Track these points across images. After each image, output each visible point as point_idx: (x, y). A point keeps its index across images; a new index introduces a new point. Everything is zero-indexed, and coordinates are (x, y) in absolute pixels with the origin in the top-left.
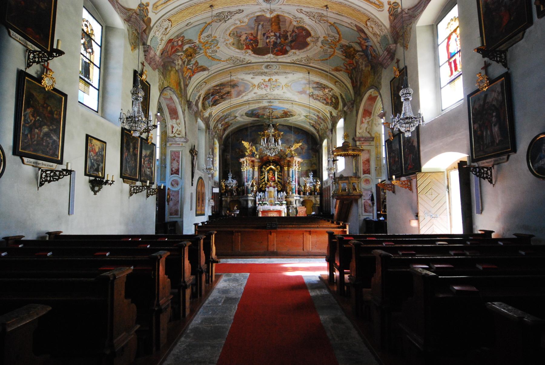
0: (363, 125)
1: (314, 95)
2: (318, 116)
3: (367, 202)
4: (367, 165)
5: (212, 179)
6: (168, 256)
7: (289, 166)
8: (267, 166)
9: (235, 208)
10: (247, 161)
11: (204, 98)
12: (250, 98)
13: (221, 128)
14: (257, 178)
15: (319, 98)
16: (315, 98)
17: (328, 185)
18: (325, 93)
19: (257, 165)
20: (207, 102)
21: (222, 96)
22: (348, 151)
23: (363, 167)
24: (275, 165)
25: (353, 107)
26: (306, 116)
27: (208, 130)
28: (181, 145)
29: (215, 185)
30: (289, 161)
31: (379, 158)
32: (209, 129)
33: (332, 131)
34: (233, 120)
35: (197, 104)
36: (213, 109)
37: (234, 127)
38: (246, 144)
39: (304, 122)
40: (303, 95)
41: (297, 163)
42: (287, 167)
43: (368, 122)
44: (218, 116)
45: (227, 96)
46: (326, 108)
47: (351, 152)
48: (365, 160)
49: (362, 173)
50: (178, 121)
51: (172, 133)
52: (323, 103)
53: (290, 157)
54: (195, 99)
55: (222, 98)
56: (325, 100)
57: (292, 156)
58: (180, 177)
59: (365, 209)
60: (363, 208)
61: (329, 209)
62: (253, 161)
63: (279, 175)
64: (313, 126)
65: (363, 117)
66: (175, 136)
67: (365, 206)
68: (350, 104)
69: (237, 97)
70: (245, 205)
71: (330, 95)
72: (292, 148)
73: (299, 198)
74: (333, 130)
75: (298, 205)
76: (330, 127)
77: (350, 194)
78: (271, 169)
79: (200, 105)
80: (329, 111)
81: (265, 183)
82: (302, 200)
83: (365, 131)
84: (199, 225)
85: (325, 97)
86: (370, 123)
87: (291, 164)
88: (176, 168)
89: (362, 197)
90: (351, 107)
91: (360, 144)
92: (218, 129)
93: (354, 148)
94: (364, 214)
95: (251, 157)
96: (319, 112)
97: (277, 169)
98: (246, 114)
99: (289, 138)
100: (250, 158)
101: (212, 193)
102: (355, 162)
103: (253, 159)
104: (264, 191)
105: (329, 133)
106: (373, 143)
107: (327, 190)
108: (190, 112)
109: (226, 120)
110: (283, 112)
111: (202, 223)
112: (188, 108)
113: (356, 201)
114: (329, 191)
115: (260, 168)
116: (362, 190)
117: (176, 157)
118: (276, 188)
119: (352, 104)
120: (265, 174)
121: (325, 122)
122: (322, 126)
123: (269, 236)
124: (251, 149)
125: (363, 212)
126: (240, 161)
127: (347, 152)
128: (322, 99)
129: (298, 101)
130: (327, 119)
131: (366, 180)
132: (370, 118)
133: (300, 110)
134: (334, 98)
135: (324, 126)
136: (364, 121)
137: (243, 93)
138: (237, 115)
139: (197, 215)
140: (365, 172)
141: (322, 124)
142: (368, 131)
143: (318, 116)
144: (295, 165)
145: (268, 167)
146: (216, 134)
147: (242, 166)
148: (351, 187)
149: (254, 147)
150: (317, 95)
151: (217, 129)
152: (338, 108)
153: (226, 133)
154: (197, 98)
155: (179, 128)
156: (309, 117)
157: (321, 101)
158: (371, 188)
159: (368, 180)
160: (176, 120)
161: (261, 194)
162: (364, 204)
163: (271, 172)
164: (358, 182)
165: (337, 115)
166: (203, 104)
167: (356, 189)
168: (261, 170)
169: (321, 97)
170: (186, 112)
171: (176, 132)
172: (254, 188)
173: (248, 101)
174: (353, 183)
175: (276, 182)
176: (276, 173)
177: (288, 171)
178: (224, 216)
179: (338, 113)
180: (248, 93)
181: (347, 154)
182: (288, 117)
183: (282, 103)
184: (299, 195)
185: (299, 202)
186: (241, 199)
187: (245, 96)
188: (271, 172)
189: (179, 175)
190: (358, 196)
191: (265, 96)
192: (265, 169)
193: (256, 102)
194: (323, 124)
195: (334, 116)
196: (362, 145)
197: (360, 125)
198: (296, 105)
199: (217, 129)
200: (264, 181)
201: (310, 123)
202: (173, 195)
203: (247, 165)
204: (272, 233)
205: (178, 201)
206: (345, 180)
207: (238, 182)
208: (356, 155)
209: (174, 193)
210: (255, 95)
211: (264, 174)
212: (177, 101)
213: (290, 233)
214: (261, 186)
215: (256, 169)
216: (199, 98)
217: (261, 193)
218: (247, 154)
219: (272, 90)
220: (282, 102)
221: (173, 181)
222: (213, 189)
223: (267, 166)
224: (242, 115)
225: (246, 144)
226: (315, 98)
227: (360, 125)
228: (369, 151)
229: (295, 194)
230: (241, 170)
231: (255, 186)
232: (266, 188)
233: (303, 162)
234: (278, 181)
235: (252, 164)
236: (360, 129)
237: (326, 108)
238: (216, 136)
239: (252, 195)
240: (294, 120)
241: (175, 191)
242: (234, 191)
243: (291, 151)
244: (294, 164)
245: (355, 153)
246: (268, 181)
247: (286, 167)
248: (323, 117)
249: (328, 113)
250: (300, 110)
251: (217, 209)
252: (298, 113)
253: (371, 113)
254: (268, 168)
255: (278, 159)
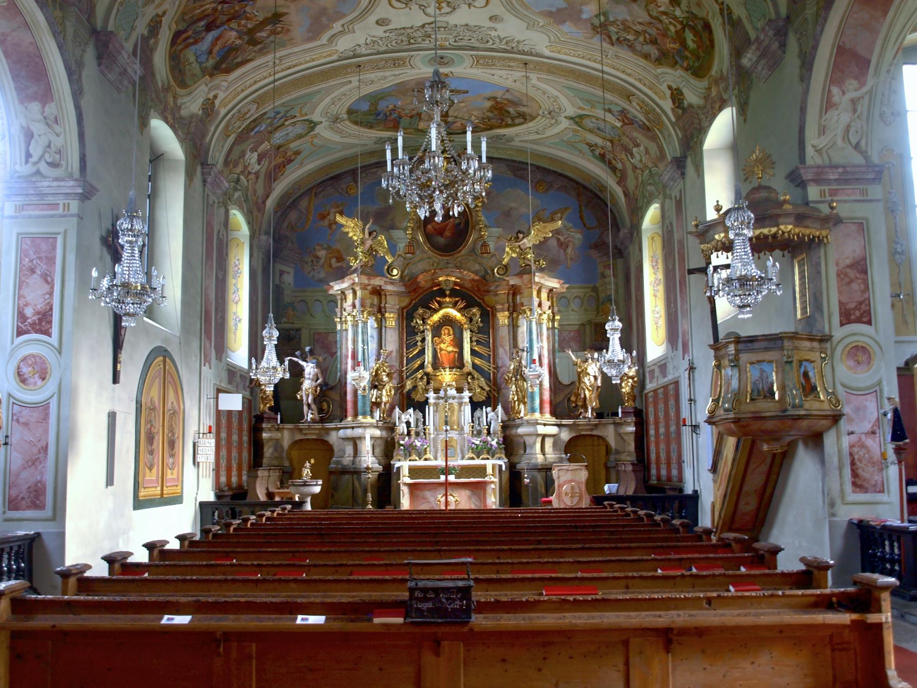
0: (833, 114)
1: (614, 23)
2: (623, 115)
3: (863, 446)
4: (855, 286)
5: (219, 357)
6: (620, 339)
7: (515, 310)
8: (430, 308)
9: (306, 472)
10: (355, 293)
11: (177, 35)
12: (362, 42)
13: (257, 167)
14: (394, 354)
15: (630, 37)
16: (614, 38)
17: (670, 377)
18: (655, 14)
19: (393, 305)
20: (190, 55)
21: (251, 32)
22: (777, 225)
23: (840, 293)
24: (461, 305)
25: (783, 45)
26: (578, 120)
27: (199, 169)
28: (60, 211)
29: (230, 382)
30: (515, 291)
31: (901, 254)
32: (204, 164)
33: (680, 163)
34: (300, 136)
35: (145, 52)
36: (218, 87)
37: (310, 166)
38: (352, 228)
39: (571, 144)
40: (568, 27)
41: (544, 295)
42: (507, 313)
43: (854, 102)
44: (242, 116)
45: (274, 32)
46: (657, 77)
47: (790, 227)
48: (848, 262)
49: (836, 319)
50: (51, 109)
51: (27, 162)
52: (646, 57)
53: (520, 274)
54: (133, 28)
55: (253, 42)
56: (654, 42)
57: (526, 271)
58: (56, 344)
59: (855, 474)
60: (847, 472)
61: (674, 472)
62: (378, 292)
63: (478, 342)
64: (602, 157)
65: (833, 81)
66: (38, 172)
67: (853, 463)
68: (771, 33)
69: (309, 40)
70: (347, 460)
71: (675, 18)
72: (525, 240)
73: (554, 430)
74: (689, 163)
75: (551, 455)
76: (673, 148)
77: (791, 412)
78: (447, 321)
79: (160, 59)
80: (670, 88)
81: (427, 374)
82: (565, 436)
83: (840, 143)
84: (167, 547)
85: (653, 32)
86: (862, 108)
87: (525, 301)
88: (40, 306)
89: (843, 422)
90: (775, 45)
91: (822, 194)
92: (246, 172)
93: (801, 210)
94: (852, 497)
95: (370, 276)
96: (628, 96)
97: (471, 320)
98: (350, 112)
99: (513, 205)
100: (365, 280)
101: (218, 413)
102: (802, 278)
103: (378, 282)
104: (421, 406)
105: (667, 173)
106: (876, 191)
107: (666, 394)
108: (111, 77)
109: (278, 137)
110: (488, 104)
111: (181, 538)
112: (100, 58)
113: (816, 440)
114: (672, 402)
115: (407, 316)
116: (840, 391)
117: (40, 258)
118: (467, 394)
119: (781, 34)
120: (423, 340)
121: (654, 138)
122: (638, 157)
123: (428, 658)
124: (369, 243)
125: (848, 487)
126: (331, 292)
127: (774, 230)
128: (641, 39)
129: (547, 52)
130: (660, 123)
131: (856, 347)
132: (862, 84)
133: (556, 93)
134: (693, 29)
135: (647, 152)
136: (836, 99)
137: (335, 21)
138: (316, 117)
139: (139, 504)
140: (847, 318)
141: (638, 145)
142: (854, 141)
143: (623, 115)
144: (540, 305)
145: (436, 311)
146: (235, 189)
147: (338, 310)
148: (794, 378)
149: (382, 238)
150: (624, 22)
151: (240, 169)
152: (709, 68)
153: (280, 188)
154: (142, 28)
155: (53, 138)
156: (587, 123)
157: (638, 47)
158: (879, 383)
159: (864, 349)
160: (44, 104)
161: (411, 415)
162: (851, 454)
163: (447, 338)
164: (823, 359)
165: (706, 98)
166: (176, 61)
167: (814, 389)
168: (408, 326)
169: (637, 33)
170: (85, 73)
171: (42, 157)
172: (384, 392)
173: (355, 56)
174: (800, 362)
175: (466, 370)
176: (467, 335)
177: (514, 327)
178: (264, 506)
179: (709, 89)
180: (352, 22)
181: (774, 236)
182: (507, 126)
183: (487, 65)
184: (553, 420)
185: (555, 445)
186: (333, 438)
187: (341, 33)
188: (447, 338)
189: (49, 335)
190: (825, 417)
191: (419, 34)
192: (423, 320)
193: (386, 60)
194: (642, 148)
195: (690, 106)
196: (832, 201)
197: (821, 117)
198: (540, 70)
199: (240, 169)
200: (422, 366)
201: (590, 145)
202: (22, 420)
203: (354, 306)
204: (445, 644)
205: (45, 449)
206: (767, 349)
207: (322, 372)
208: (812, 241)
209: (26, 412)
210: (379, 32)
211: (419, 338)
212: (41, 17)
213: (546, 644)
214: (409, 385)
215: (391, 320)
216: (155, 26)
217: (411, 411)
218: (354, 264)
219: (446, 9)
220: (484, 57)
221: (24, 359)
222: (220, 395)
223: (430, 308)
224: (336, 119)
225: (352, 228)
226: (614, 38)
227: (821, 117)
228: (862, 227)
229: (541, 412)
230: (335, 324)
231: (387, 387)
232: (427, 391)
233: (568, 295)
234: (474, 366)
235: (376, 301)
236: (822, 131)
237: (657, 77)
238: (237, 195)
239: (374, 421)
240: (531, 137)
241: (33, 406)
242: (309, 405)
243: (522, 252)
244: (536, 301)
245: (807, 231)
246: (436, 364)
247: (503, 310)
248: (646, 114)
249: (663, 97)
250: (556, 93)
251: (240, 476)
252: (547, 105)
253: (868, 62)
254: (436, 317)
255: (473, 280)
